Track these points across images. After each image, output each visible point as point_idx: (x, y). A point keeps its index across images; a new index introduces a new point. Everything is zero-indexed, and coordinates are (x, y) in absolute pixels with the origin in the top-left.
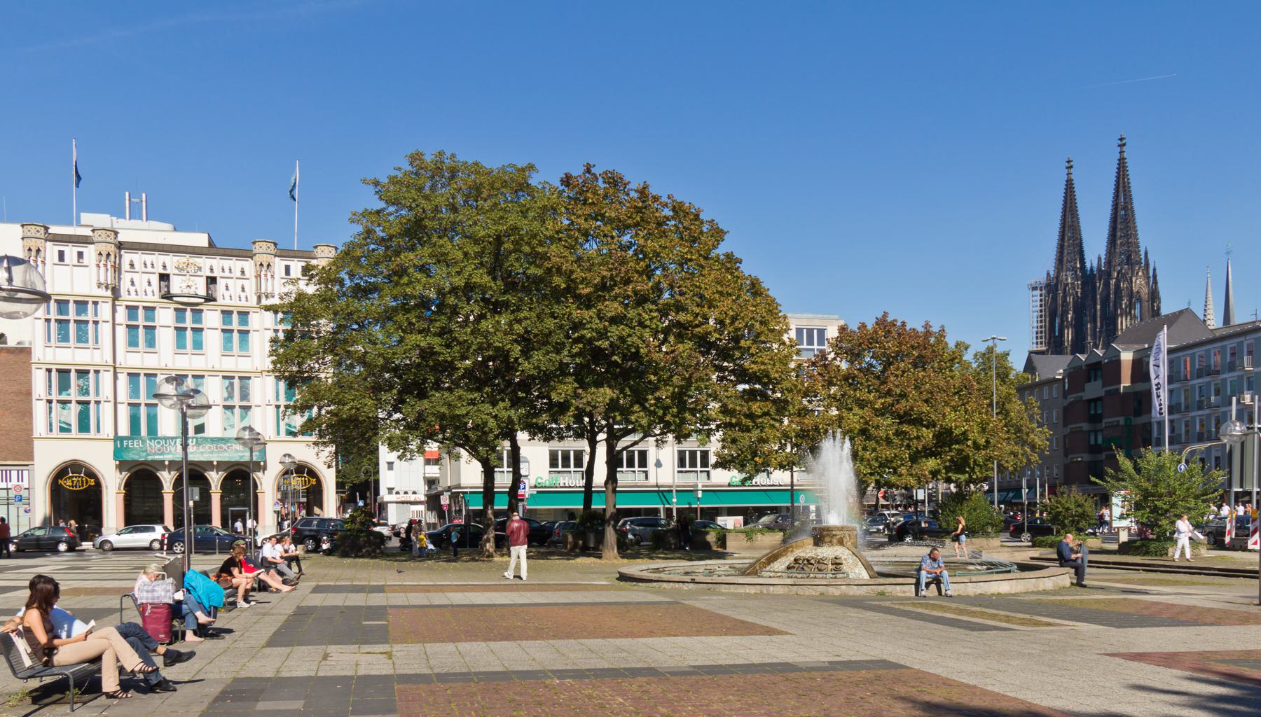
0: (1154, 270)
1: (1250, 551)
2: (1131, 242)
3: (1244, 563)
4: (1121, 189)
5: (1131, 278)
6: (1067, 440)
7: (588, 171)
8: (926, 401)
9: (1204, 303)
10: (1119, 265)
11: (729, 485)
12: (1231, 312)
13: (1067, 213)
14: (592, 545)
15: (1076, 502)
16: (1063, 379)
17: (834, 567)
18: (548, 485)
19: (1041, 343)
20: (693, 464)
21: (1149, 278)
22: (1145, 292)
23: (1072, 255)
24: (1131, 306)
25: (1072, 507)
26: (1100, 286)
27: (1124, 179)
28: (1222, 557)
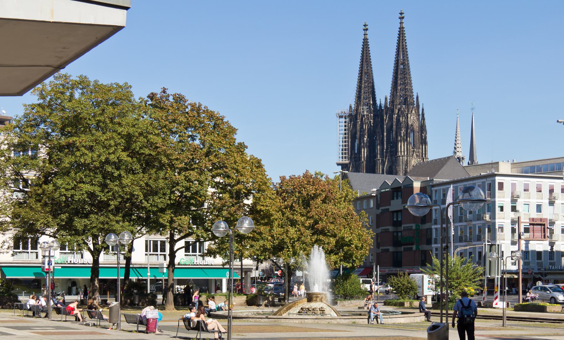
0: (423, 110)
1: (494, 308)
2: (407, 89)
3: (493, 313)
4: (401, 49)
5: (407, 114)
7: (164, 92)
8: (332, 223)
9: (455, 135)
10: (399, 104)
12: (474, 149)
13: (364, 63)
14: (137, 303)
16: (376, 196)
17: (321, 312)
18: (60, 262)
19: (345, 158)
20: (155, 250)
21: (419, 115)
22: (416, 126)
23: (367, 95)
24: (407, 135)
26: (386, 118)
27: (403, 43)
28: (483, 311)
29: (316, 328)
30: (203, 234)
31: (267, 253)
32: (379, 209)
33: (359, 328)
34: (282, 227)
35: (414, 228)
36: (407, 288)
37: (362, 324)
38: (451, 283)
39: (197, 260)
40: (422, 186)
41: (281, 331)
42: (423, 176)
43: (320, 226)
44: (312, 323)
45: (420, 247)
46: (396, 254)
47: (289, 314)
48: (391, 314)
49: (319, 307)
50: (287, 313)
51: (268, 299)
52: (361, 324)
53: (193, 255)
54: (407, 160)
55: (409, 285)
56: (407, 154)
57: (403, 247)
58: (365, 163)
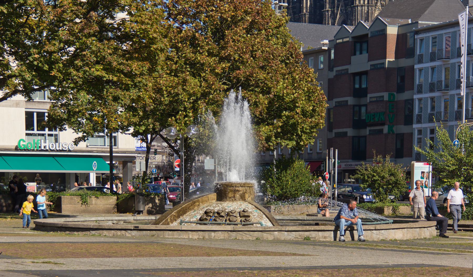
6: (332, 113)
8: (263, 68)
11: (17, 149)
15: (390, 171)
17: (243, 219)
25: (387, 176)
29: (232, 247)
30: (23, 74)
31: (150, 120)
32: (333, 71)
33: (322, 248)
34: (176, 76)
35: (386, 98)
36: (388, 183)
37: (323, 242)
38: (469, 173)
39: (45, 142)
40: (400, 33)
41: (152, 255)
42: (402, 18)
43: (242, 73)
44: (224, 240)
45: (394, 129)
46: (357, 139)
47: (181, 223)
48: (383, 222)
49: (238, 210)
50: (179, 221)
51: (152, 201)
52: (320, 242)
53: (39, 135)
54: (368, 12)
55: (392, 178)
56: (368, 3)
57: (368, 129)
58: (307, 16)
